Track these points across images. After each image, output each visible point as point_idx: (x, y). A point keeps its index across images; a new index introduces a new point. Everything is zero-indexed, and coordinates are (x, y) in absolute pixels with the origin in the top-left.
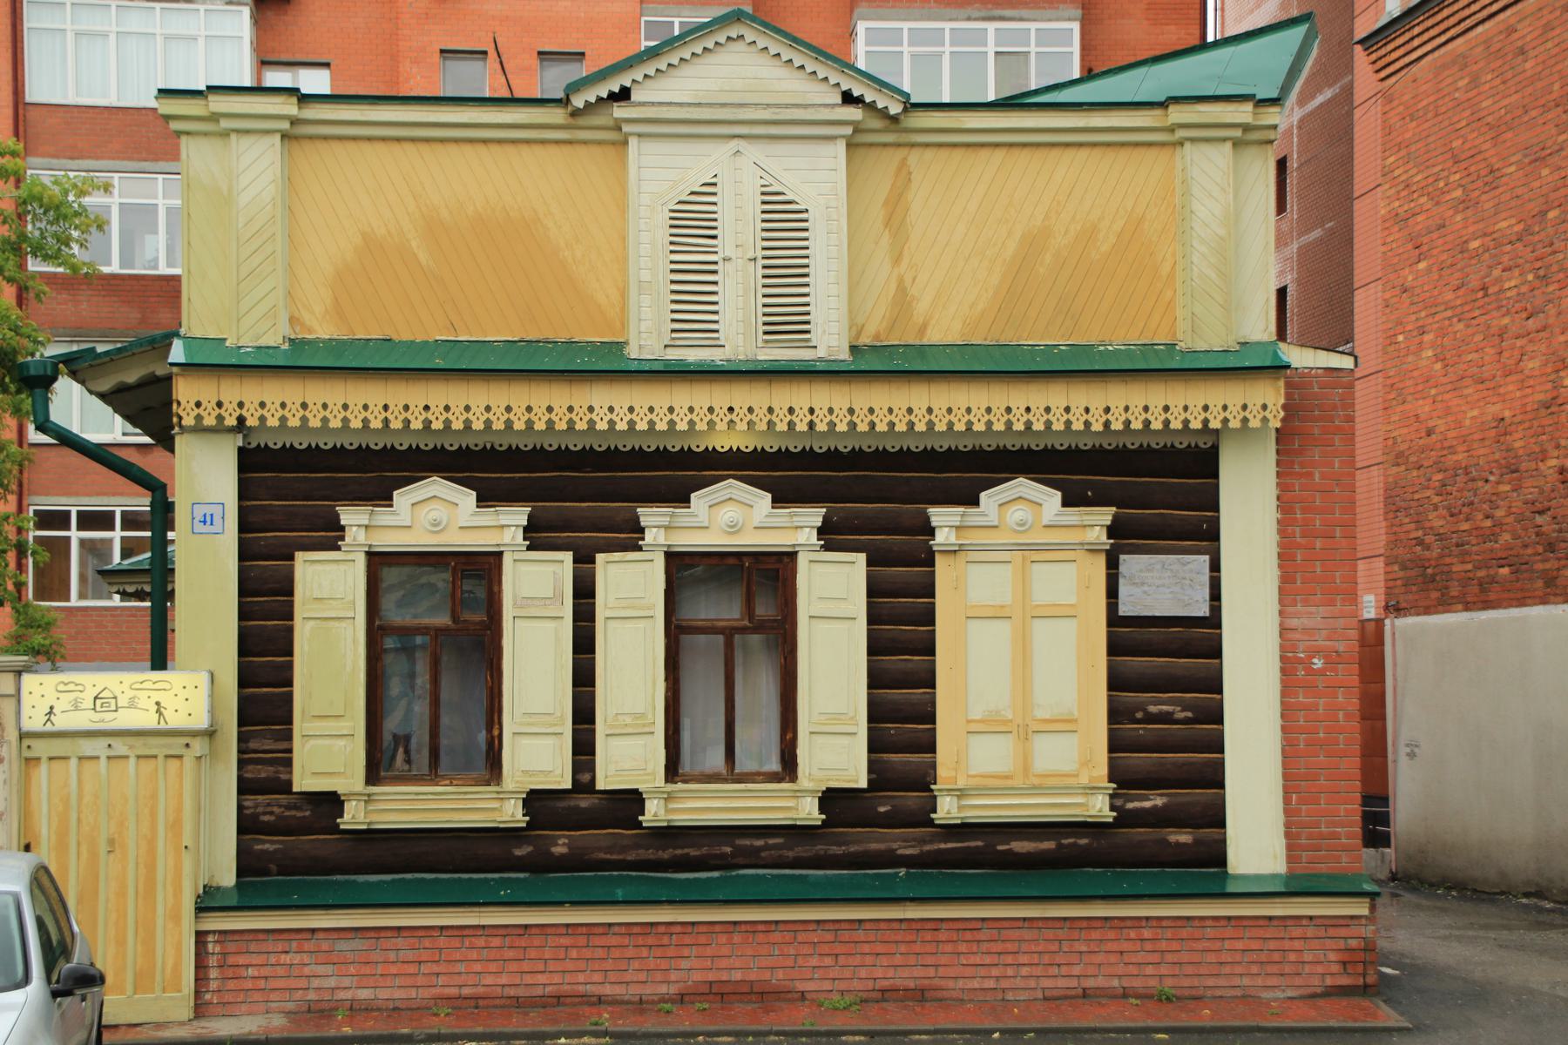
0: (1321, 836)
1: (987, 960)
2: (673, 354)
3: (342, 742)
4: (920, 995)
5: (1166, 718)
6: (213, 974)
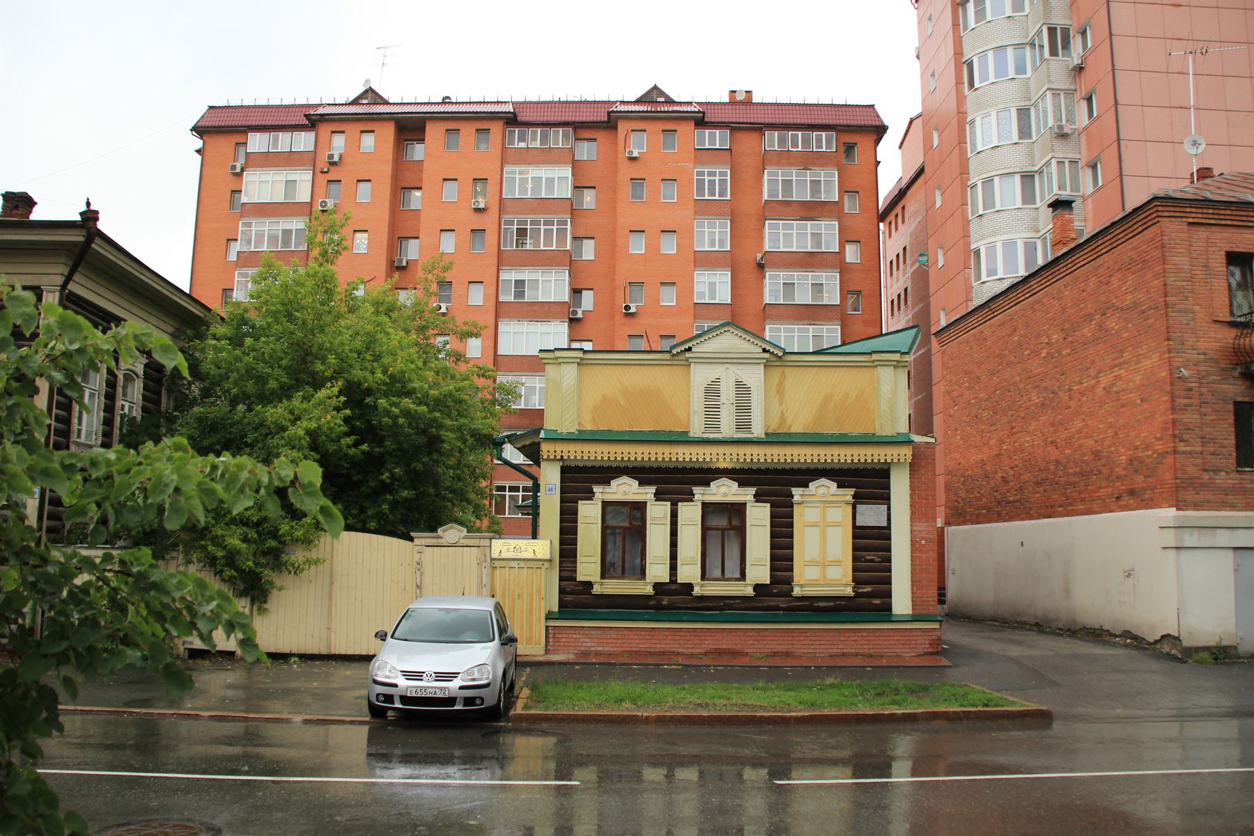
0: (924, 601)
1: (810, 643)
2: (705, 436)
3: (593, 565)
4: (787, 654)
6: (551, 640)
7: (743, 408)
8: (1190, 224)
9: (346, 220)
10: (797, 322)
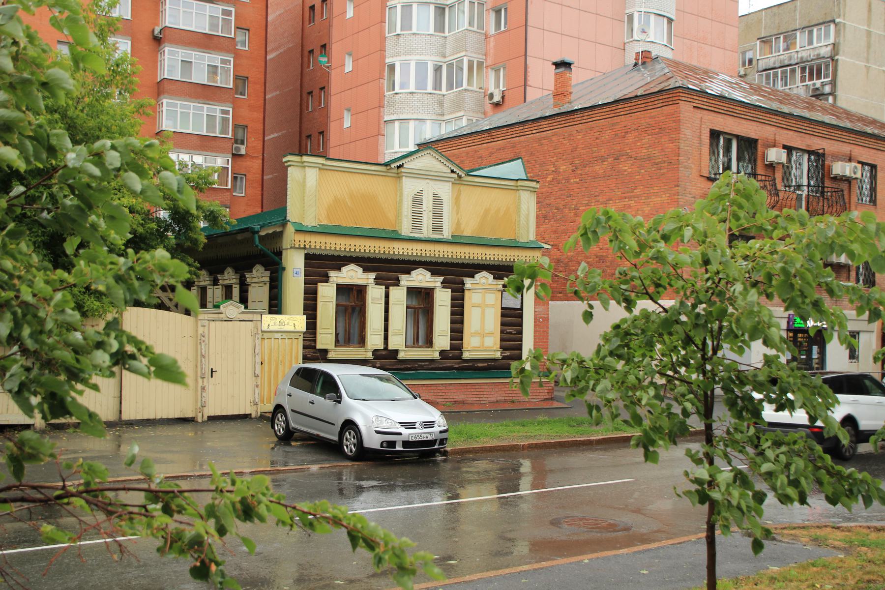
2: (412, 235)
3: (329, 335)
4: (463, 402)
5: (510, 333)
7: (437, 215)
8: (694, 107)
9: (626, 132)
10: (193, 100)
